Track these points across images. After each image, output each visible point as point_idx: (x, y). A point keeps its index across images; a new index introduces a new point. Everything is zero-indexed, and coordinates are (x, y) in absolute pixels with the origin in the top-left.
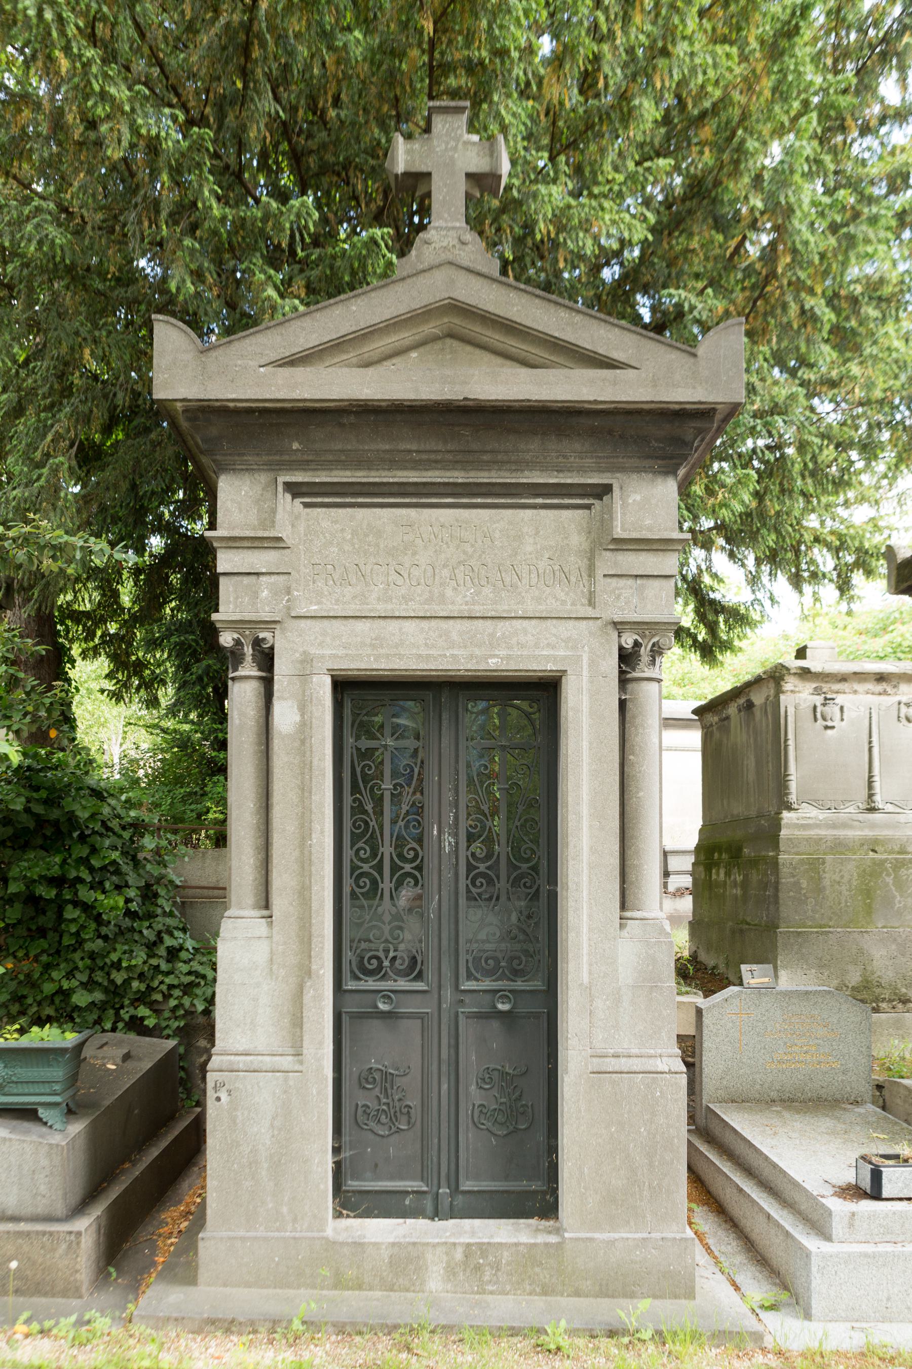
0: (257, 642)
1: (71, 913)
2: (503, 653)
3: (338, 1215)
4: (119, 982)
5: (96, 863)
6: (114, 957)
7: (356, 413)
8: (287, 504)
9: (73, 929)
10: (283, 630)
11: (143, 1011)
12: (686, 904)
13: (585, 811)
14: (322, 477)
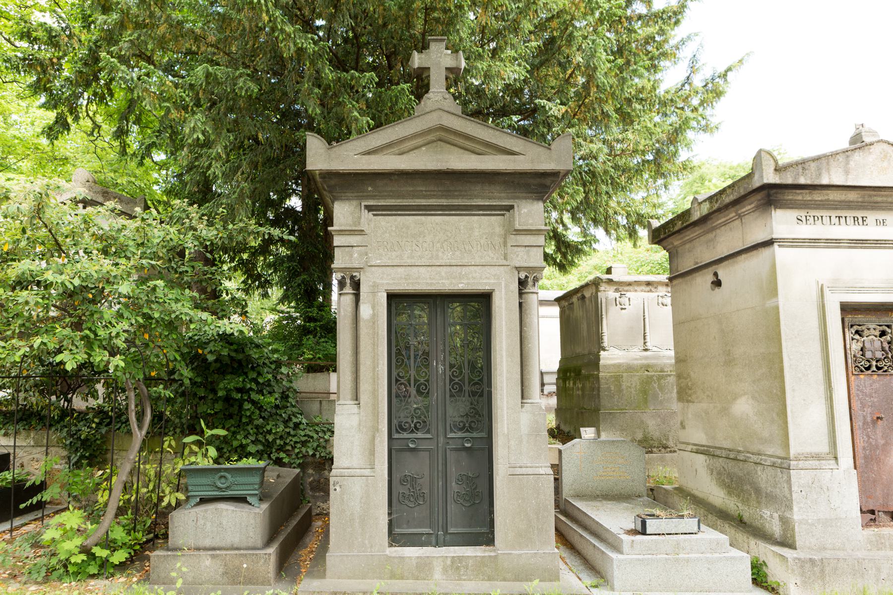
0: (352, 277)
1: (247, 406)
2: (465, 281)
3: (391, 546)
4: (270, 440)
5: (261, 380)
6: (268, 427)
7: (398, 175)
8: (366, 215)
10: (364, 272)
11: (282, 455)
12: (553, 401)
13: (504, 354)
14: (382, 203)
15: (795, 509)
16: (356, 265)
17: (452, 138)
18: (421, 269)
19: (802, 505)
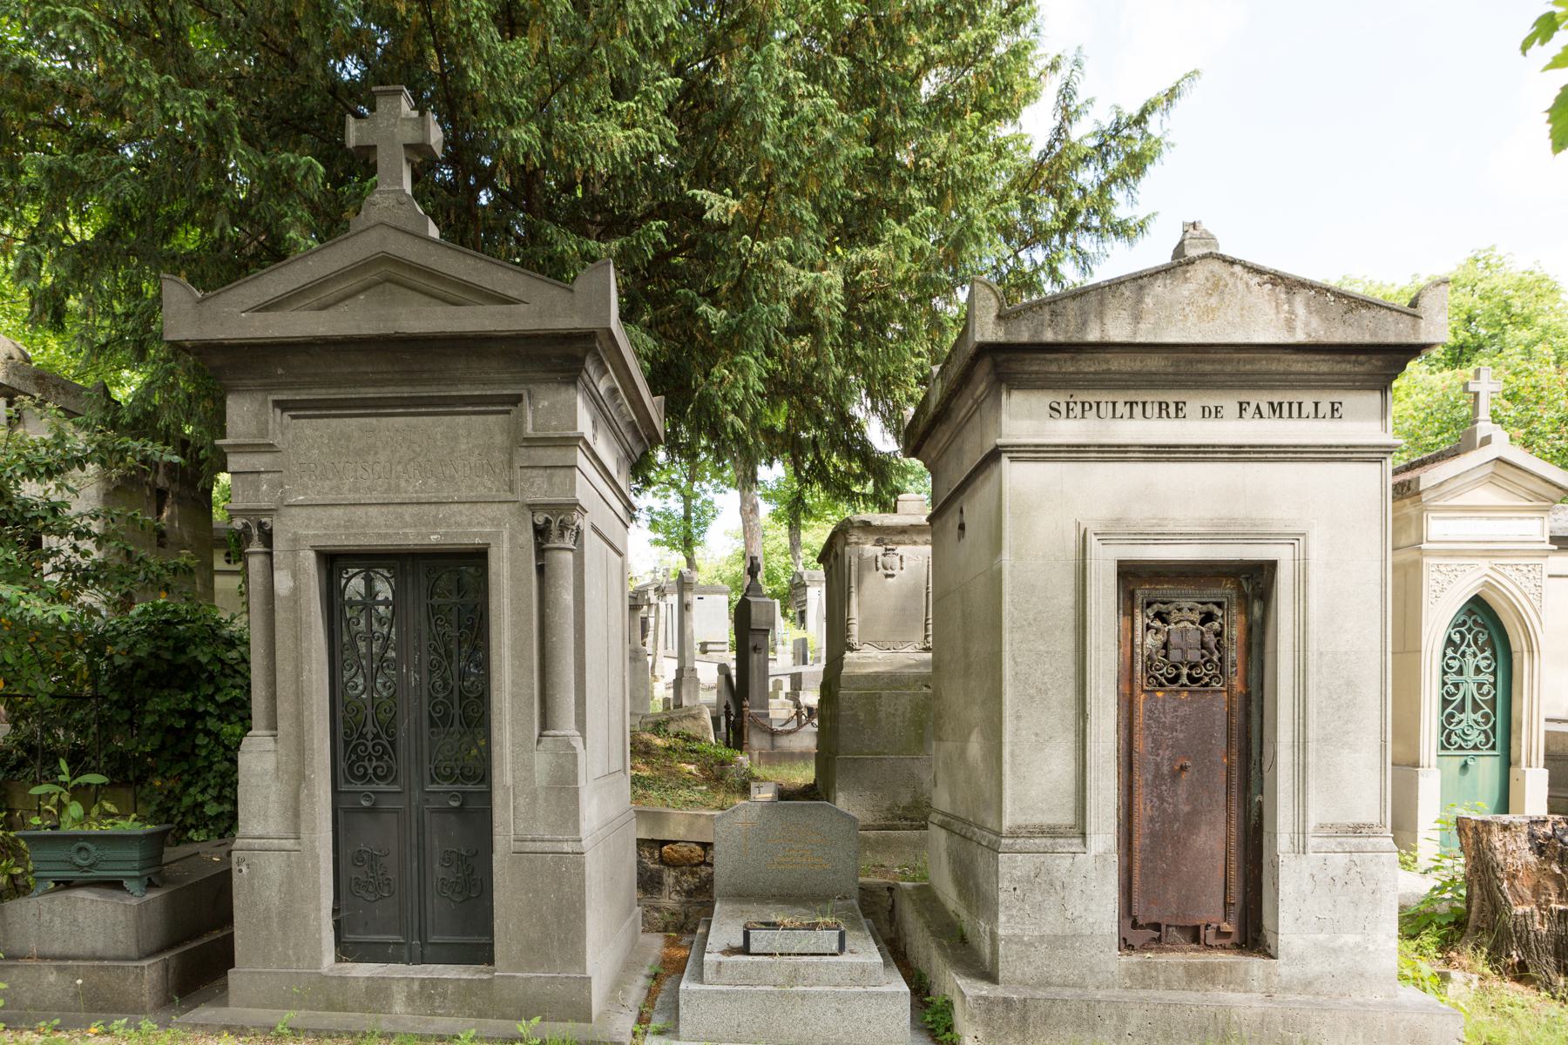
0: (261, 525)
2: (442, 531)
7: (321, 345)
8: (276, 418)
9: (204, 753)
15: (1002, 918)
16: (264, 505)
17: (406, 275)
18: (371, 509)
19: (1014, 912)
